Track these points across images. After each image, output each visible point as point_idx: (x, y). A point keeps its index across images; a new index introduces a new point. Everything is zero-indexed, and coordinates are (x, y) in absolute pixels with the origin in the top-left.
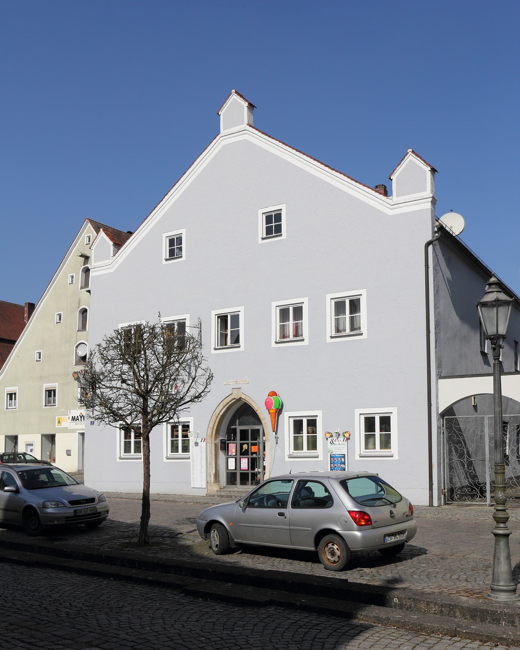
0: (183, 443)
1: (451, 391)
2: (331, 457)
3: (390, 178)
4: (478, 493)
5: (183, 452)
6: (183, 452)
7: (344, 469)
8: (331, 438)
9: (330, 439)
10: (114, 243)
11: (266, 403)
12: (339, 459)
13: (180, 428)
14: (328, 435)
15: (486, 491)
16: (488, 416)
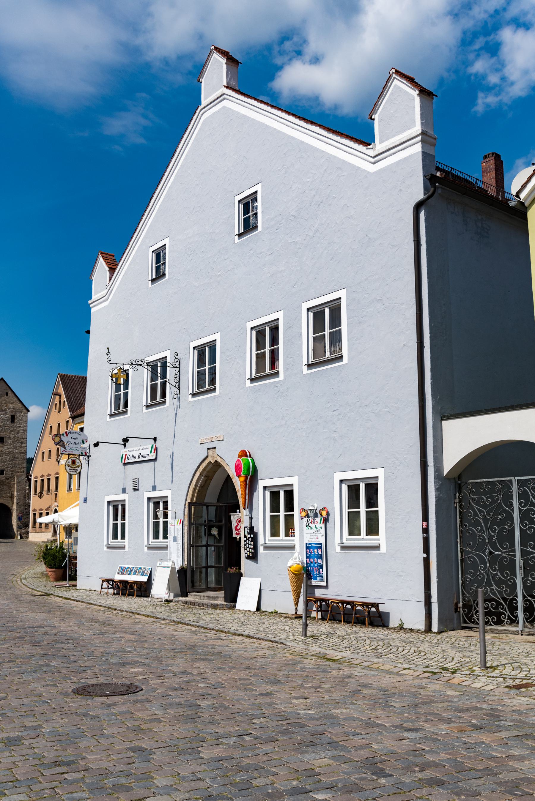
0: (368, 520)
1: (465, 437)
2: (307, 548)
3: (371, 118)
4: (505, 610)
5: (121, 539)
6: (121, 539)
7: (118, 574)
8: (306, 519)
9: (306, 520)
10: (109, 268)
11: (236, 466)
12: (316, 550)
13: (161, 504)
14: (304, 514)
15: (516, 608)
16: (517, 478)
